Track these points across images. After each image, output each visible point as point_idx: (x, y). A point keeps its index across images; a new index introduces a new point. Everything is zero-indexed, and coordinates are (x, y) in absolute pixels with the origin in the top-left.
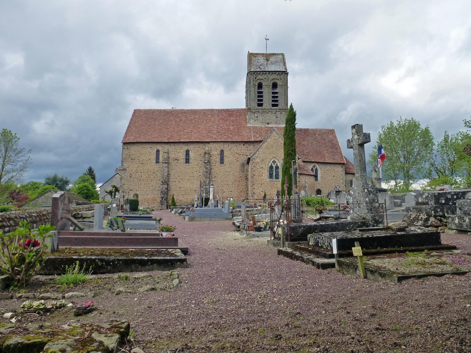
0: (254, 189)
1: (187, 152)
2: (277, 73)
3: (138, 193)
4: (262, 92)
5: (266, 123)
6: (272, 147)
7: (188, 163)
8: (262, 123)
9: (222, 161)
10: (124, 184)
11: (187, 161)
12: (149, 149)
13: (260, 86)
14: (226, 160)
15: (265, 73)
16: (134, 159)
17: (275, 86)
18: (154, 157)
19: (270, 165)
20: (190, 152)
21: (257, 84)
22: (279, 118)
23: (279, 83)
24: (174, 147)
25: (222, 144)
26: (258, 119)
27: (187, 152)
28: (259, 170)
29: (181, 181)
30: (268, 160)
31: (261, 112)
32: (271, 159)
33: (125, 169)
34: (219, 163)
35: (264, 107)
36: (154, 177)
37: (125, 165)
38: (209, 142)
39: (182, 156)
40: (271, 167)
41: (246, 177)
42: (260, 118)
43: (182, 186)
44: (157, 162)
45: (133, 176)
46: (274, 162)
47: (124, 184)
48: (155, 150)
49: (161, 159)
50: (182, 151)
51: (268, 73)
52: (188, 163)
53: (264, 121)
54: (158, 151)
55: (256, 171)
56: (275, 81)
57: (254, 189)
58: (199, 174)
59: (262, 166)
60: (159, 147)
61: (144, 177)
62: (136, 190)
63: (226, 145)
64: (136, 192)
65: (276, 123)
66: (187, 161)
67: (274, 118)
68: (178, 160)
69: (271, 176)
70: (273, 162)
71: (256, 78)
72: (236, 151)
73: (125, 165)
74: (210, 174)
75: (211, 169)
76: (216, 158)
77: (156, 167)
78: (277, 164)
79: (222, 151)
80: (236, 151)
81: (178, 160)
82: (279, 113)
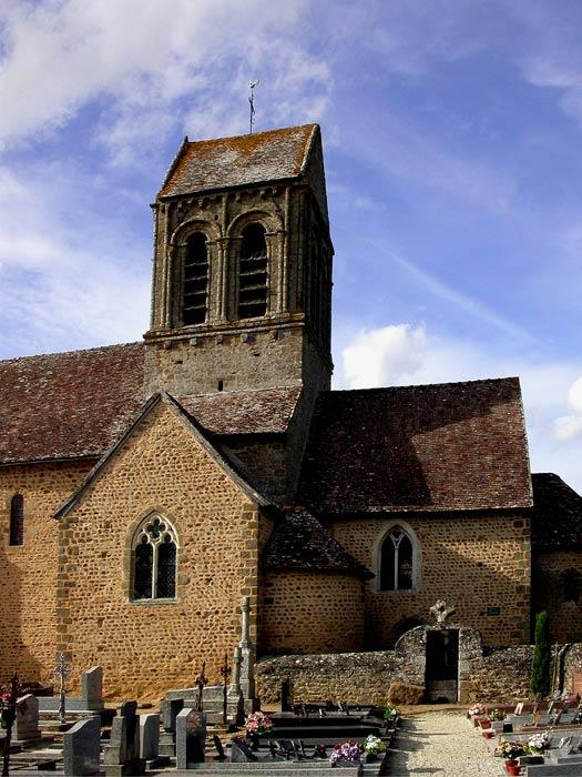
15: (213, 197)
69: (139, 588)
78: (167, 537)
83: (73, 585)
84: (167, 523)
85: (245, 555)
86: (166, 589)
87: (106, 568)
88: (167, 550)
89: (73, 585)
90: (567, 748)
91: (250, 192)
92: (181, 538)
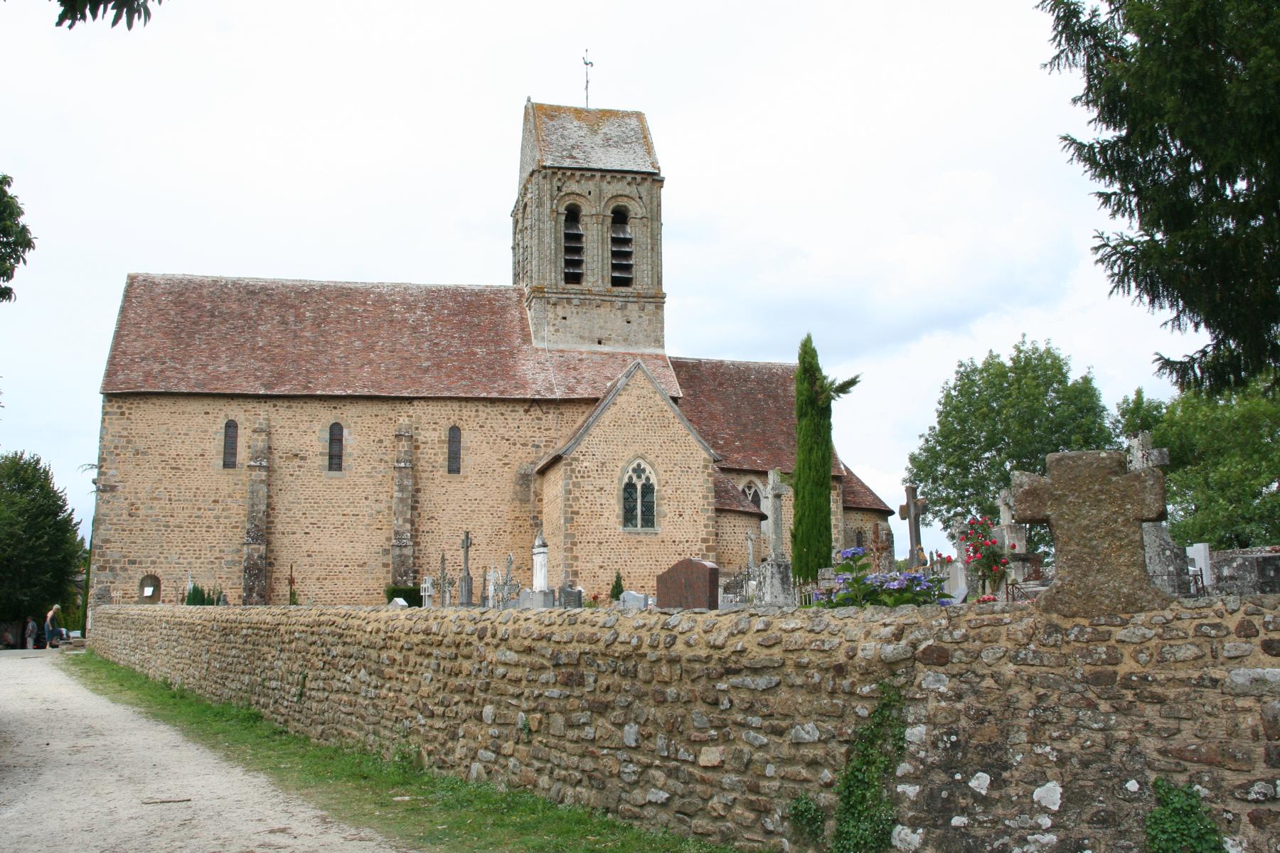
0: (576, 558)
1: (336, 434)
2: (629, 177)
3: (159, 572)
4: (627, 241)
5: (592, 340)
6: (633, 421)
7: (339, 468)
8: (581, 337)
9: (454, 466)
10: (108, 541)
11: (335, 460)
12: (201, 419)
13: (573, 215)
14: (467, 460)
15: (589, 174)
16: (144, 453)
17: (620, 217)
18: (216, 445)
19: (626, 480)
20: (345, 432)
21: (562, 210)
22: (634, 326)
23: (635, 209)
24: (289, 413)
25: (456, 405)
26: (566, 327)
27: (336, 434)
28: (591, 498)
29: (315, 532)
30: (620, 464)
31: (576, 302)
32: (630, 462)
33: (113, 488)
34: (443, 471)
35: (585, 285)
36: (217, 517)
37: (111, 472)
38: (410, 400)
39: (317, 443)
40: (630, 487)
41: (535, 518)
42: (574, 321)
43: (316, 547)
44: (229, 463)
45: (141, 512)
46: (639, 471)
47: (108, 541)
48: (222, 423)
49: (242, 455)
50: (317, 427)
51: (598, 175)
52: (339, 468)
53: (587, 334)
54: (231, 427)
55: (582, 501)
56: (622, 202)
57: (576, 558)
58: (377, 506)
59: (599, 483)
60: (235, 411)
61: (181, 517)
62: (153, 563)
63: (468, 411)
64: (152, 570)
65: (625, 340)
66: (335, 460)
67: (620, 322)
68: (303, 458)
69: (628, 518)
70: (634, 470)
71: (559, 189)
72: (502, 431)
73: (111, 472)
74: (414, 508)
75: (418, 491)
76: (434, 452)
77: (225, 482)
78: (648, 479)
79: (455, 432)
80: (502, 431)
81: (303, 458)
82: (635, 307)
83: (577, 513)
84: (648, 469)
85: (706, 497)
86: (649, 520)
87: (603, 501)
88: (648, 489)
89: (577, 513)
90: (236, 506)
91: (619, 176)
92: (659, 481)
